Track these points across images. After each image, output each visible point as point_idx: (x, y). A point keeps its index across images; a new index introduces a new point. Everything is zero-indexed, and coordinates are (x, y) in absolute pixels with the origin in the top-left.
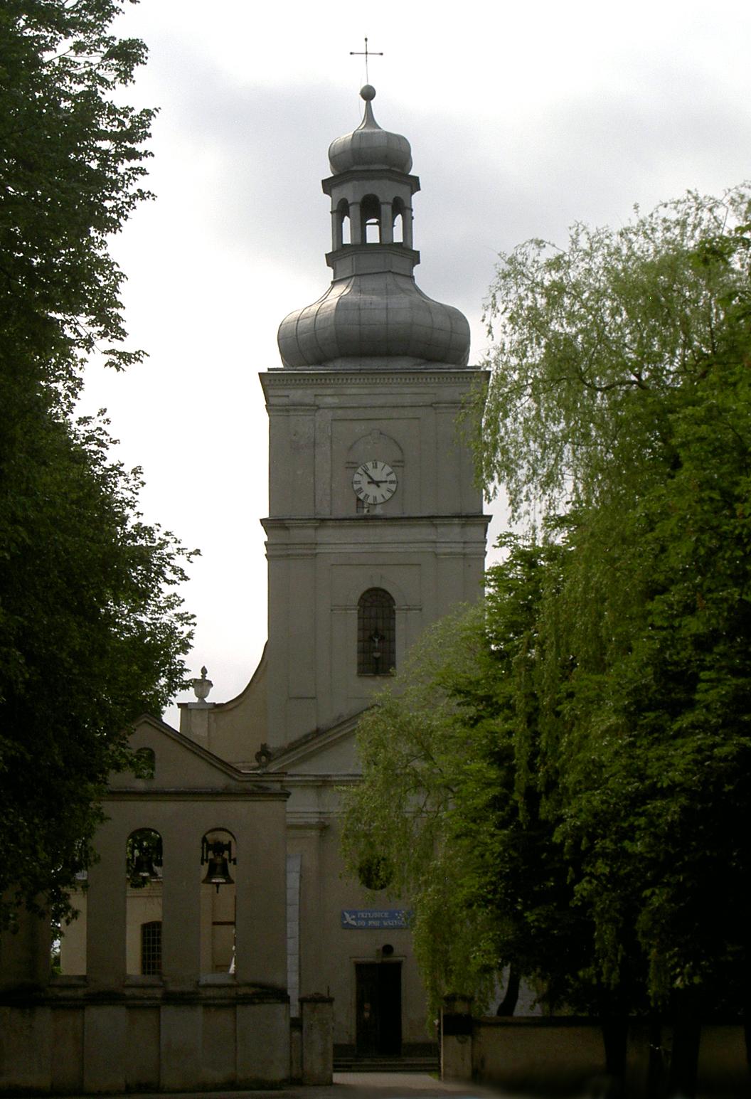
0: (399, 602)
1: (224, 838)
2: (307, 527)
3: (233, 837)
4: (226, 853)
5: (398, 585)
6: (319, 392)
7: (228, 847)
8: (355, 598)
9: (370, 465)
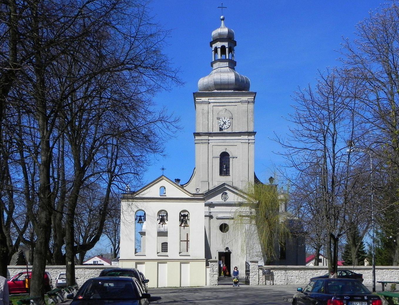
0: (231, 156)
1: (186, 213)
2: (207, 296)
3: (189, 213)
4: (187, 217)
5: (231, 151)
6: (209, 98)
7: (187, 216)
8: (218, 155)
9: (223, 118)
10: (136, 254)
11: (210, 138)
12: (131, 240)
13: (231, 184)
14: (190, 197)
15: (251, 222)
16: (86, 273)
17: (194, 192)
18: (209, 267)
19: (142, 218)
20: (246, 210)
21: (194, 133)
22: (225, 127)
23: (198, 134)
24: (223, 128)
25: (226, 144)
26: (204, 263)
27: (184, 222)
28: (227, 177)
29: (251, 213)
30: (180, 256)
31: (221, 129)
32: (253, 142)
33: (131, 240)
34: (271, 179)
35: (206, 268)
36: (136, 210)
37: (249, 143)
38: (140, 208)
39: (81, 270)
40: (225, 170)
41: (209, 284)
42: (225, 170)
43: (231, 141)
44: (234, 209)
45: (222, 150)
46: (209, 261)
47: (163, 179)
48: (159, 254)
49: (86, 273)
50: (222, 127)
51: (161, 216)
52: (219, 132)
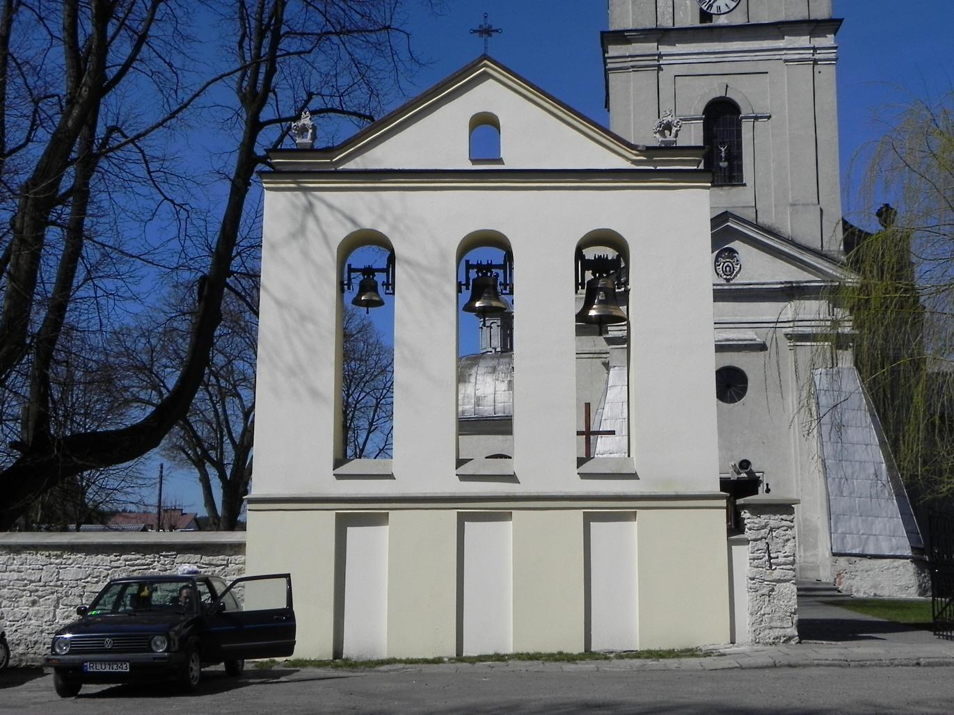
5: (745, 93)
8: (698, 108)
10: (340, 471)
11: (664, 49)
12: (315, 394)
13: (750, 215)
14: (628, 166)
15: (834, 363)
16: (70, 574)
17: (656, 140)
18: (747, 542)
19: (380, 278)
20: (812, 310)
21: (603, 33)
22: (719, 8)
23: (621, 37)
24: (714, 10)
25: (726, 68)
26: (718, 518)
27: (601, 296)
28: (735, 190)
29: (836, 323)
30: (584, 476)
31: (705, 16)
32: (833, 56)
33: (315, 394)
34: (885, 213)
35: (731, 543)
36: (340, 232)
37: (815, 62)
38: (367, 222)
39: (41, 558)
40: (724, 164)
41: (750, 637)
42: (724, 164)
43: (749, 56)
44: (767, 311)
45: (712, 89)
46: (744, 507)
47: (485, 76)
48: (467, 469)
49: (70, 574)
50: (711, 6)
51: (479, 267)
52: (699, 25)
